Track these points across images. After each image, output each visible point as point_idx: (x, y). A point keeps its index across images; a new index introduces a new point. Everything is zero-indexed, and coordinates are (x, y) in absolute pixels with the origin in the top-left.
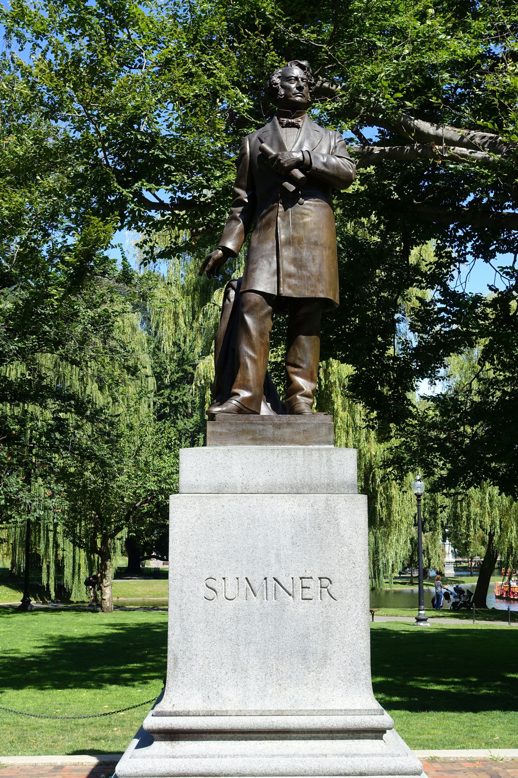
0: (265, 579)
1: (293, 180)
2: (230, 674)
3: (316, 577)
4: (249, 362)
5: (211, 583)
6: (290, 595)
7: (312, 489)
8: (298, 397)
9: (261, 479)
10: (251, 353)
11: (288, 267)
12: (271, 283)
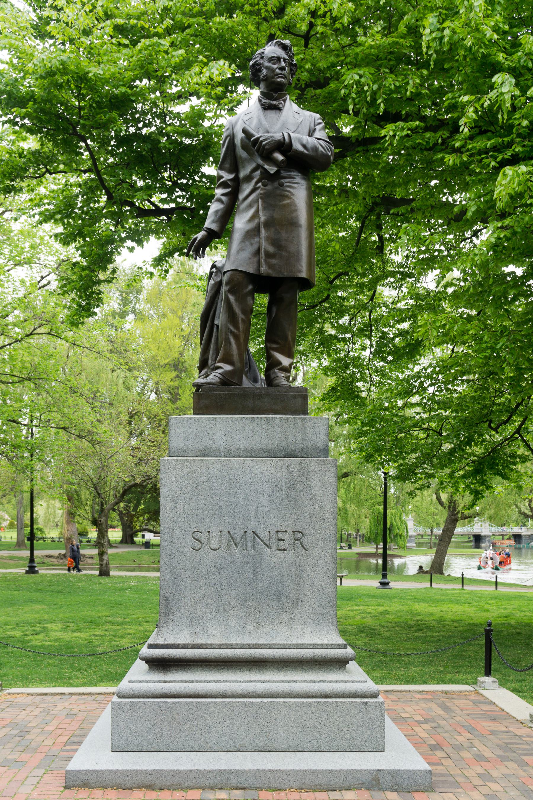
2: (213, 614)
3: (290, 531)
6: (267, 546)
9: (242, 444)
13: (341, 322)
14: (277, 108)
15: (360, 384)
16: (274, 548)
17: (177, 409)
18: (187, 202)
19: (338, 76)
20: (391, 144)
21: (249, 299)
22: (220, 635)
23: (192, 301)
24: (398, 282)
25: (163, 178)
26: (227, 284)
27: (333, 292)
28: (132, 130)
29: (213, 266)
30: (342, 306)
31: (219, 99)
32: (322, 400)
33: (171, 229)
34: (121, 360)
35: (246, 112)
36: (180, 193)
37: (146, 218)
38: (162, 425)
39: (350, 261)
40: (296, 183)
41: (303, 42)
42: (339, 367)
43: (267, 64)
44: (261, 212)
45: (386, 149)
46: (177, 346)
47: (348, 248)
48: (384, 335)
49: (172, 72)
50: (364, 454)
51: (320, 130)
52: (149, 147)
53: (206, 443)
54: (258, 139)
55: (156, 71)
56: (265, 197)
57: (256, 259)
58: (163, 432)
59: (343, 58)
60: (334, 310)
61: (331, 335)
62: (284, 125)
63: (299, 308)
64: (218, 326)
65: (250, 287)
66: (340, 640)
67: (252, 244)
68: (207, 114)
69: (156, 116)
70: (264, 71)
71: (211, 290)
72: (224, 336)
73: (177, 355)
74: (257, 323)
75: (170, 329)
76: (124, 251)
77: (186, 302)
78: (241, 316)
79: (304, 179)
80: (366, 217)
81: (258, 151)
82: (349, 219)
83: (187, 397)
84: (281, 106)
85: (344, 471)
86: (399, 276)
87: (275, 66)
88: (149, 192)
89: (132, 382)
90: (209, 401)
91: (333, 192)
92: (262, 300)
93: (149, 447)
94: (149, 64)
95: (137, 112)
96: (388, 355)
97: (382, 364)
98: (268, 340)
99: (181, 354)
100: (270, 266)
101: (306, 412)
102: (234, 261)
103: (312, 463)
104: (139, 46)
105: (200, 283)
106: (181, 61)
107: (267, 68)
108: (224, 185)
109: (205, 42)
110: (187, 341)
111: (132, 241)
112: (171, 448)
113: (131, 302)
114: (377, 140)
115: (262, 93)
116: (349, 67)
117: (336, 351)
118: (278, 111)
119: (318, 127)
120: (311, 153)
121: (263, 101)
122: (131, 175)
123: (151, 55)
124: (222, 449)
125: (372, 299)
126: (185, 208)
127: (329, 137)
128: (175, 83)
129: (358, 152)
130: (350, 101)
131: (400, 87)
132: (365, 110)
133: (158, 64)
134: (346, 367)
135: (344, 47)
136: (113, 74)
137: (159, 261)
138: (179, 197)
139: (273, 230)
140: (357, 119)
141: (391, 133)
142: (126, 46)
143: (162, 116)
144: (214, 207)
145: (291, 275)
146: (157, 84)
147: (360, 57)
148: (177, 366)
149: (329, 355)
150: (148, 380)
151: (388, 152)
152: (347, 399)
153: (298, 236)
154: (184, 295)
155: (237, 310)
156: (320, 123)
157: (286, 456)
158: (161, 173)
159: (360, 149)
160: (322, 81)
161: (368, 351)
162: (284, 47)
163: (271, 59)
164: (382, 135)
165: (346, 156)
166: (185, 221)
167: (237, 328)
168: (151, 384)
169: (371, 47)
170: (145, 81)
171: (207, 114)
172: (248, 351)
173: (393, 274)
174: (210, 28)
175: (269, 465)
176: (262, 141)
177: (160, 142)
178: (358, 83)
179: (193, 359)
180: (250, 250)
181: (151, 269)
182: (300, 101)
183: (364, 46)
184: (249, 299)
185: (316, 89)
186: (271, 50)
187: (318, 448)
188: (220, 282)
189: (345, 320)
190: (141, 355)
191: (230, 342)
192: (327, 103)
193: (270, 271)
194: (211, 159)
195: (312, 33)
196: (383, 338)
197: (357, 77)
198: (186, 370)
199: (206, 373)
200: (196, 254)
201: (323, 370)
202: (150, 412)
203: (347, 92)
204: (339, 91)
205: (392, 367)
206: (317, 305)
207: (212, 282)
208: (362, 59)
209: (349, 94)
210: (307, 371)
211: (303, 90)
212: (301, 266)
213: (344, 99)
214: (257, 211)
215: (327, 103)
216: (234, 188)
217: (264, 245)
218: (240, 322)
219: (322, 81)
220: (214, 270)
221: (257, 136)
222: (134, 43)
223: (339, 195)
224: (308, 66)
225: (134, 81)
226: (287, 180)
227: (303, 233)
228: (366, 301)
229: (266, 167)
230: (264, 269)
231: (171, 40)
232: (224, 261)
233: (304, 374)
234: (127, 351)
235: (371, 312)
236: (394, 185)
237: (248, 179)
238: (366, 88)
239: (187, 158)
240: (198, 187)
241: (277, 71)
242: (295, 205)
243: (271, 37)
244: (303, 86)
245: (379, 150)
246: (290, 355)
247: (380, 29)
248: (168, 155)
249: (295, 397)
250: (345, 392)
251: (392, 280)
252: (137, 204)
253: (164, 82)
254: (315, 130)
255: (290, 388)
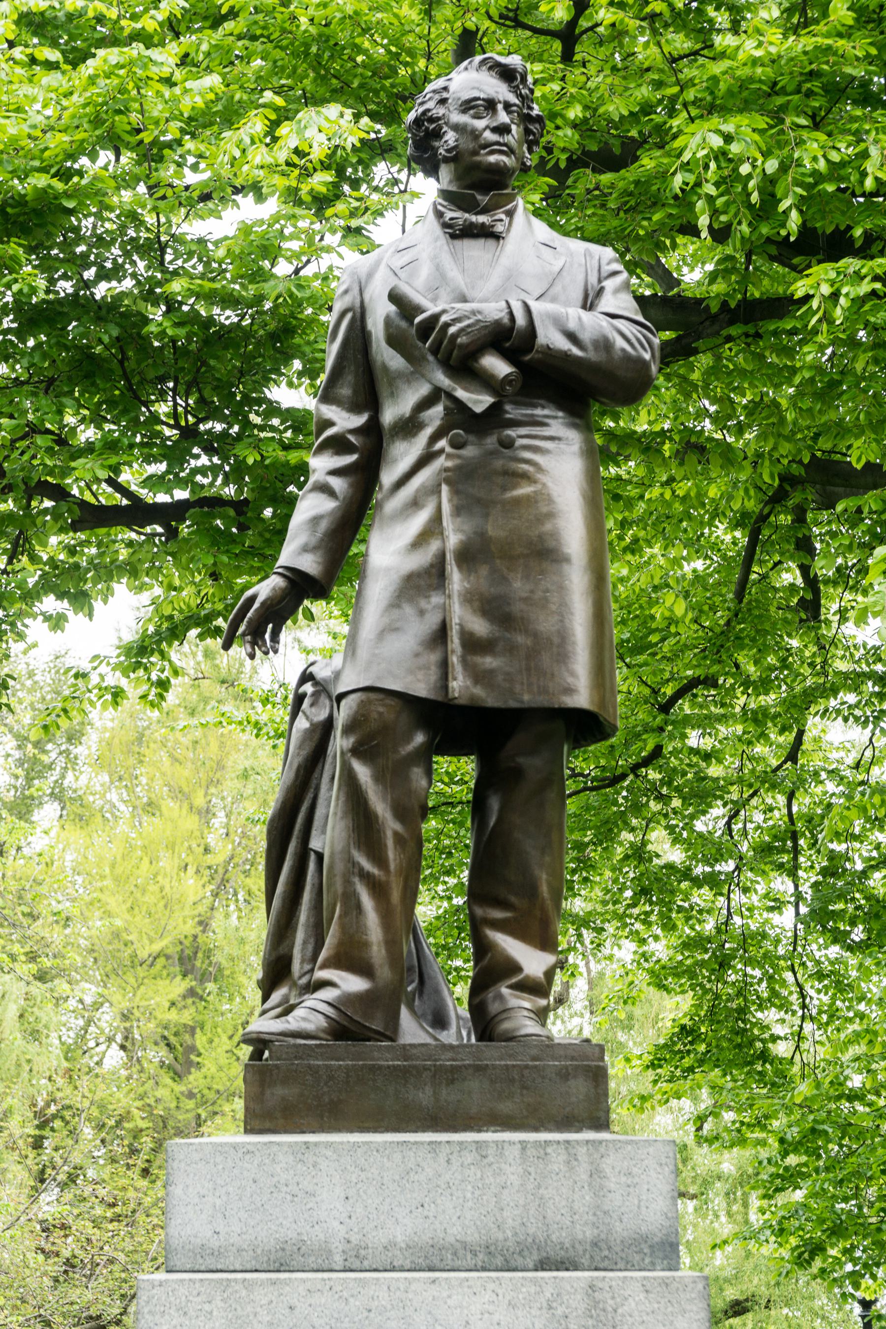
8: (505, 991)
9: (402, 1228)
12: (426, 667)
13: (699, 826)
14: (487, 233)
15: (771, 1015)
17: (191, 1095)
18: (226, 483)
19: (662, 138)
20: (827, 318)
21: (417, 774)
23: (238, 761)
24: (868, 703)
25: (155, 419)
26: (348, 730)
27: (671, 737)
28: (66, 287)
29: (306, 677)
30: (701, 778)
31: (320, 204)
32: (652, 1065)
33: (177, 563)
34: (16, 948)
35: (398, 248)
36: (204, 460)
37: (102, 531)
38: (145, 1147)
39: (720, 644)
40: (552, 438)
41: (557, 46)
42: (702, 964)
43: (457, 118)
44: (447, 521)
45: (816, 332)
46: (192, 898)
47: (713, 609)
48: (834, 867)
49: (183, 131)
50: (793, 1241)
51: (617, 291)
52: (115, 332)
53: (282, 1225)
54: (435, 317)
55: (138, 131)
56: (459, 478)
57: (434, 657)
58: (145, 1172)
59: (676, 89)
60: (678, 790)
61: (670, 867)
62: (511, 279)
63: (570, 786)
64: (320, 857)
65: (419, 738)
67: (422, 613)
68: (286, 245)
69: (135, 247)
70: (450, 137)
71: (300, 747)
72: (339, 888)
73: (189, 928)
74: (439, 833)
75: (171, 846)
76: (36, 629)
77: (220, 766)
78: (391, 825)
79: (574, 426)
80: (763, 518)
81: (435, 350)
82: (711, 524)
83: (223, 1065)
84: (499, 228)
85: (732, 1293)
86: (870, 687)
87: (480, 124)
88: (113, 460)
89: (46, 1013)
90: (291, 1090)
91: (659, 451)
92: (456, 774)
93: (96, 1223)
94: (119, 112)
95: (80, 239)
96: (853, 923)
97: (834, 951)
98: (478, 892)
99: (204, 924)
100: (479, 676)
101: (601, 1122)
102: (369, 663)
103: (628, 1287)
104: (90, 67)
105: (263, 714)
106: (208, 104)
107: (456, 128)
108: (338, 444)
109: (278, 54)
110: (221, 883)
111: (60, 596)
112: (175, 1242)
113: (50, 767)
114: (783, 305)
115: (445, 194)
116: (694, 112)
117: (688, 914)
118: (491, 243)
119: (610, 284)
120: (591, 355)
121: (449, 215)
122: (60, 412)
123: (122, 91)
124: (337, 1247)
125: (792, 756)
126: (216, 502)
127: (640, 300)
128: (191, 160)
129: (729, 339)
130: (700, 205)
131: (843, 164)
132: (745, 228)
133: (142, 112)
134: (723, 963)
135: (674, 60)
136: (14, 140)
137: (140, 652)
138: (203, 471)
139: (484, 571)
140: (721, 251)
141: (826, 289)
142: (51, 66)
143: (154, 249)
144: (311, 509)
145: (542, 701)
146: (139, 163)
147: (723, 86)
148: (191, 961)
149: (669, 926)
150: (97, 1006)
151: (820, 338)
152: (731, 1063)
153: (562, 589)
154: (214, 746)
155: (380, 807)
156: (615, 273)
157: (543, 1265)
158: (146, 404)
159: (734, 331)
160: (617, 151)
161: (789, 911)
162: (507, 74)
163: (467, 106)
164: (799, 294)
165: (695, 352)
166: (219, 540)
167: (379, 859)
168: (107, 1018)
169: (755, 62)
170: (105, 156)
171: (286, 245)
172: (412, 927)
173: (854, 680)
174: (294, 18)
175: (488, 1296)
176: (447, 325)
177: (146, 321)
178: (721, 155)
179: (242, 941)
180: (416, 628)
181: (114, 679)
182: (555, 207)
183: (733, 58)
184: (417, 774)
185: (598, 172)
186: (469, 80)
187: (645, 1239)
188: (328, 726)
189: (712, 820)
190: (77, 927)
191: (359, 907)
192: (633, 209)
193: (478, 691)
194: (297, 364)
195: (584, 23)
196: (833, 875)
197: (717, 142)
198: (218, 975)
199: (286, 999)
200: (254, 643)
201: (651, 972)
202: (102, 1107)
203: (691, 179)
204: (664, 175)
205: (868, 962)
206: (623, 776)
207: (302, 724)
208: (730, 93)
209: (698, 184)
210: (601, 975)
211: (561, 175)
212: (573, 674)
213: (685, 199)
214: (437, 518)
215: (633, 209)
216: (366, 456)
217: (462, 616)
218: (390, 843)
219: (617, 151)
220: (308, 688)
221: (432, 309)
222: (77, 58)
223: (680, 456)
224: (575, 112)
225: (73, 157)
226: (523, 431)
227: (577, 580)
228: (775, 763)
229: (461, 394)
230: (459, 685)
231: (181, 51)
232: (338, 661)
233: (591, 983)
234: (32, 916)
235: (791, 797)
236: (841, 429)
237: (409, 427)
238: (745, 169)
239: (226, 364)
240: (257, 444)
241: (489, 136)
242: (550, 500)
243: (467, 45)
244: (563, 165)
245: (793, 332)
246: (545, 941)
247: (776, 13)
248: (168, 353)
249: (564, 1075)
250: (722, 1042)
251: (851, 698)
252: (75, 491)
253: (160, 159)
254: (600, 292)
255: (548, 1046)
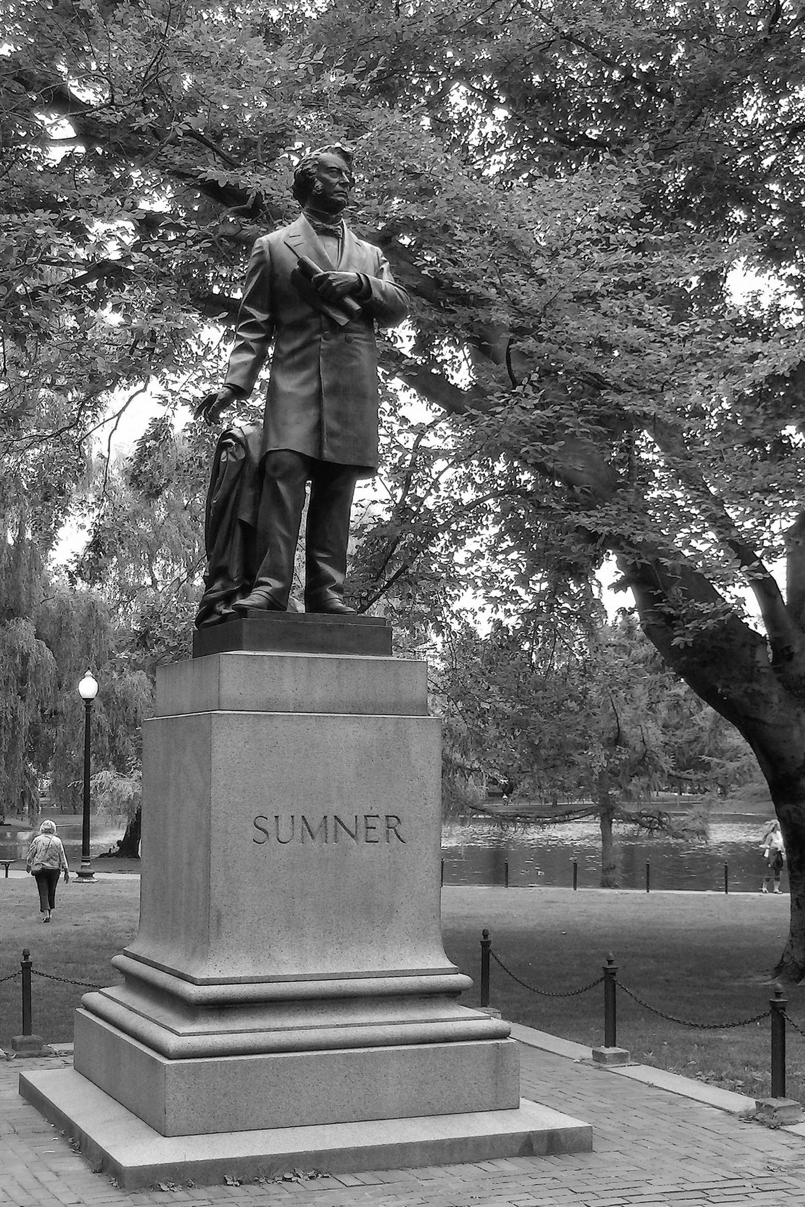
0: (325, 817)
1: (347, 311)
3: (382, 816)
4: (281, 542)
5: (262, 823)
6: (352, 836)
7: (377, 709)
8: (328, 591)
9: (319, 695)
10: (284, 532)
11: (330, 423)
16: (362, 838)
22: (297, 965)
66: (449, 965)
176: (331, 281)
